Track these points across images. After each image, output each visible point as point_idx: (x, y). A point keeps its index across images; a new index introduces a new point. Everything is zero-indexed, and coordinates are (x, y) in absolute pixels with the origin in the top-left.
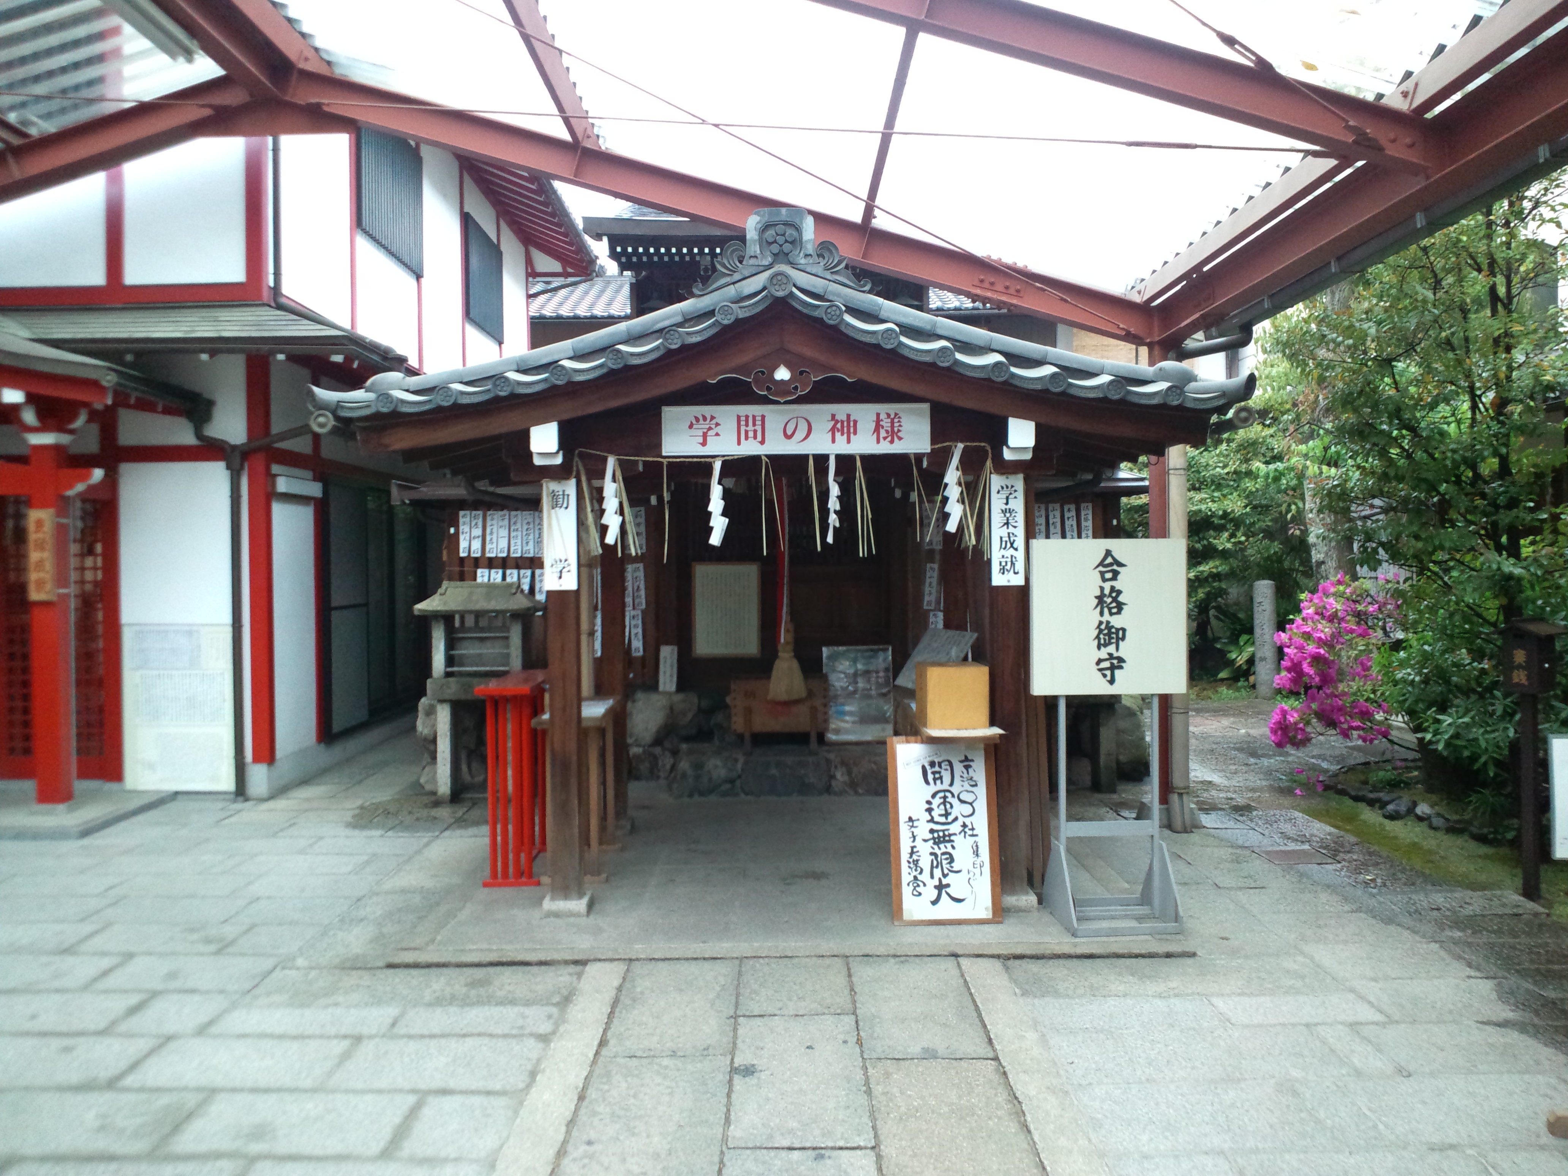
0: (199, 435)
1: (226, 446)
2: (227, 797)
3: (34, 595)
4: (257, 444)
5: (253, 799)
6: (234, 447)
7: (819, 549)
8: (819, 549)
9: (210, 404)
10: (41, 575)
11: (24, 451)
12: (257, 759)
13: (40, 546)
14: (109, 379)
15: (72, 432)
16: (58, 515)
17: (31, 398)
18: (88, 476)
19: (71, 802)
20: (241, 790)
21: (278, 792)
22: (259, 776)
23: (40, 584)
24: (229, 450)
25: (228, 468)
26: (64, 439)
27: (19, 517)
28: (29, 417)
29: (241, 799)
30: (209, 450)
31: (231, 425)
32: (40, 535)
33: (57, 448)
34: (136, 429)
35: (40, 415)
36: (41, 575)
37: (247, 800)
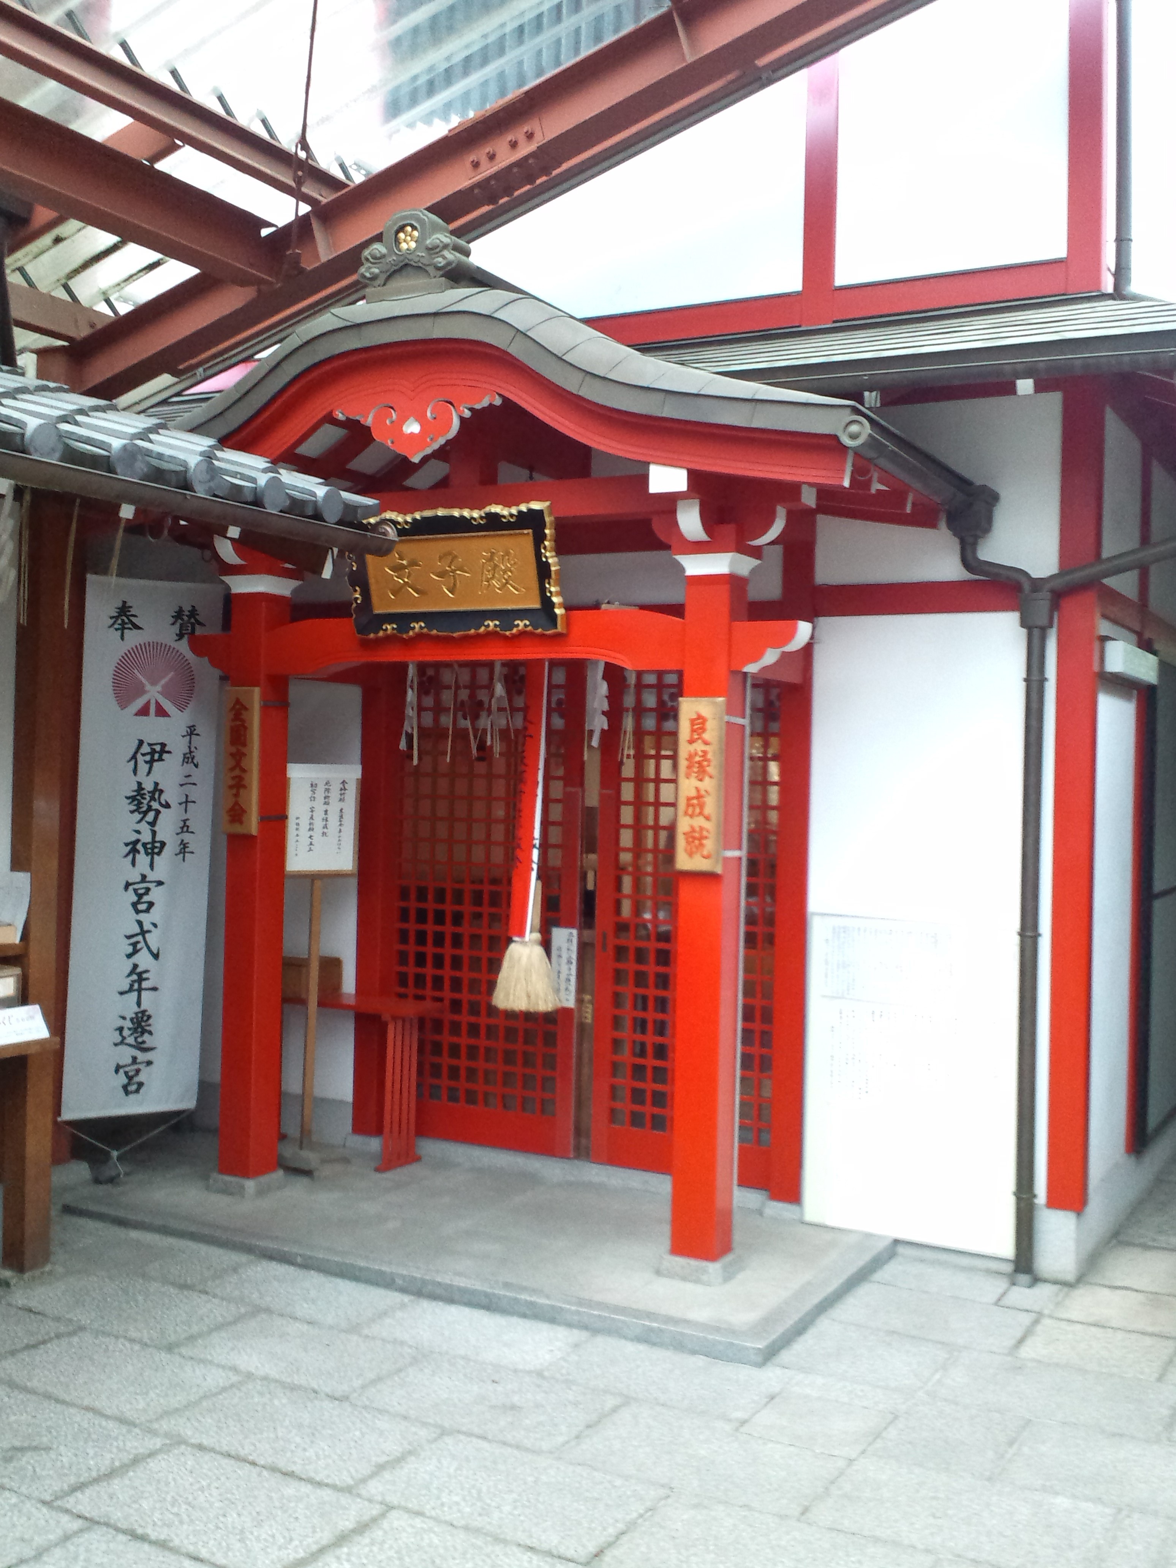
0: (968, 561)
1: (1023, 579)
2: (994, 1265)
3: (684, 862)
4: (1078, 576)
5: (1045, 1281)
6: (1037, 584)
7: (66, 626)
8: (66, 626)
9: (991, 498)
10: (699, 822)
11: (674, 595)
12: (1055, 1201)
13: (700, 769)
14: (855, 432)
15: (756, 552)
16: (730, 711)
17: (699, 481)
18: (791, 635)
19: (728, 1258)
20: (1024, 1262)
21: (1090, 1267)
22: (1061, 1237)
23: (696, 839)
24: (1026, 587)
25: (1023, 624)
26: (744, 565)
27: (668, 712)
28: (690, 522)
29: (1024, 1278)
30: (991, 588)
31: (1028, 538)
32: (699, 747)
33: (733, 582)
34: (849, 552)
35: (709, 520)
36: (699, 822)
37: (1036, 1280)
